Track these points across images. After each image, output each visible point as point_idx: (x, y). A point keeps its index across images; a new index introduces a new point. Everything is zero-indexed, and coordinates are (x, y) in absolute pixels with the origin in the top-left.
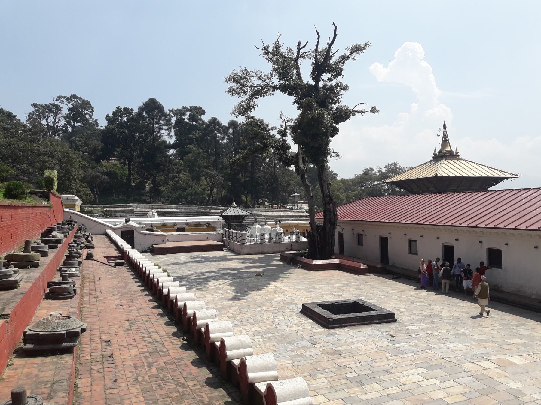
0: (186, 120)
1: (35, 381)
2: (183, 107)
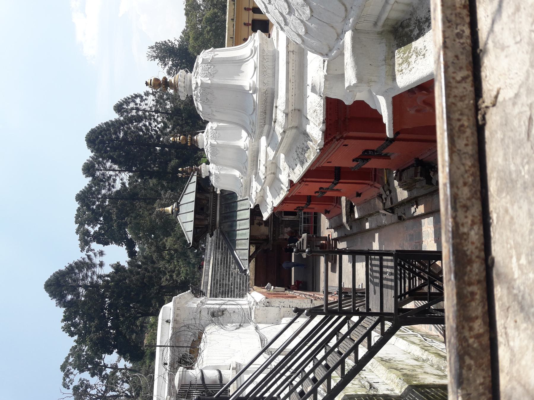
0: (97, 229)
1: (211, 30)
2: (77, 233)
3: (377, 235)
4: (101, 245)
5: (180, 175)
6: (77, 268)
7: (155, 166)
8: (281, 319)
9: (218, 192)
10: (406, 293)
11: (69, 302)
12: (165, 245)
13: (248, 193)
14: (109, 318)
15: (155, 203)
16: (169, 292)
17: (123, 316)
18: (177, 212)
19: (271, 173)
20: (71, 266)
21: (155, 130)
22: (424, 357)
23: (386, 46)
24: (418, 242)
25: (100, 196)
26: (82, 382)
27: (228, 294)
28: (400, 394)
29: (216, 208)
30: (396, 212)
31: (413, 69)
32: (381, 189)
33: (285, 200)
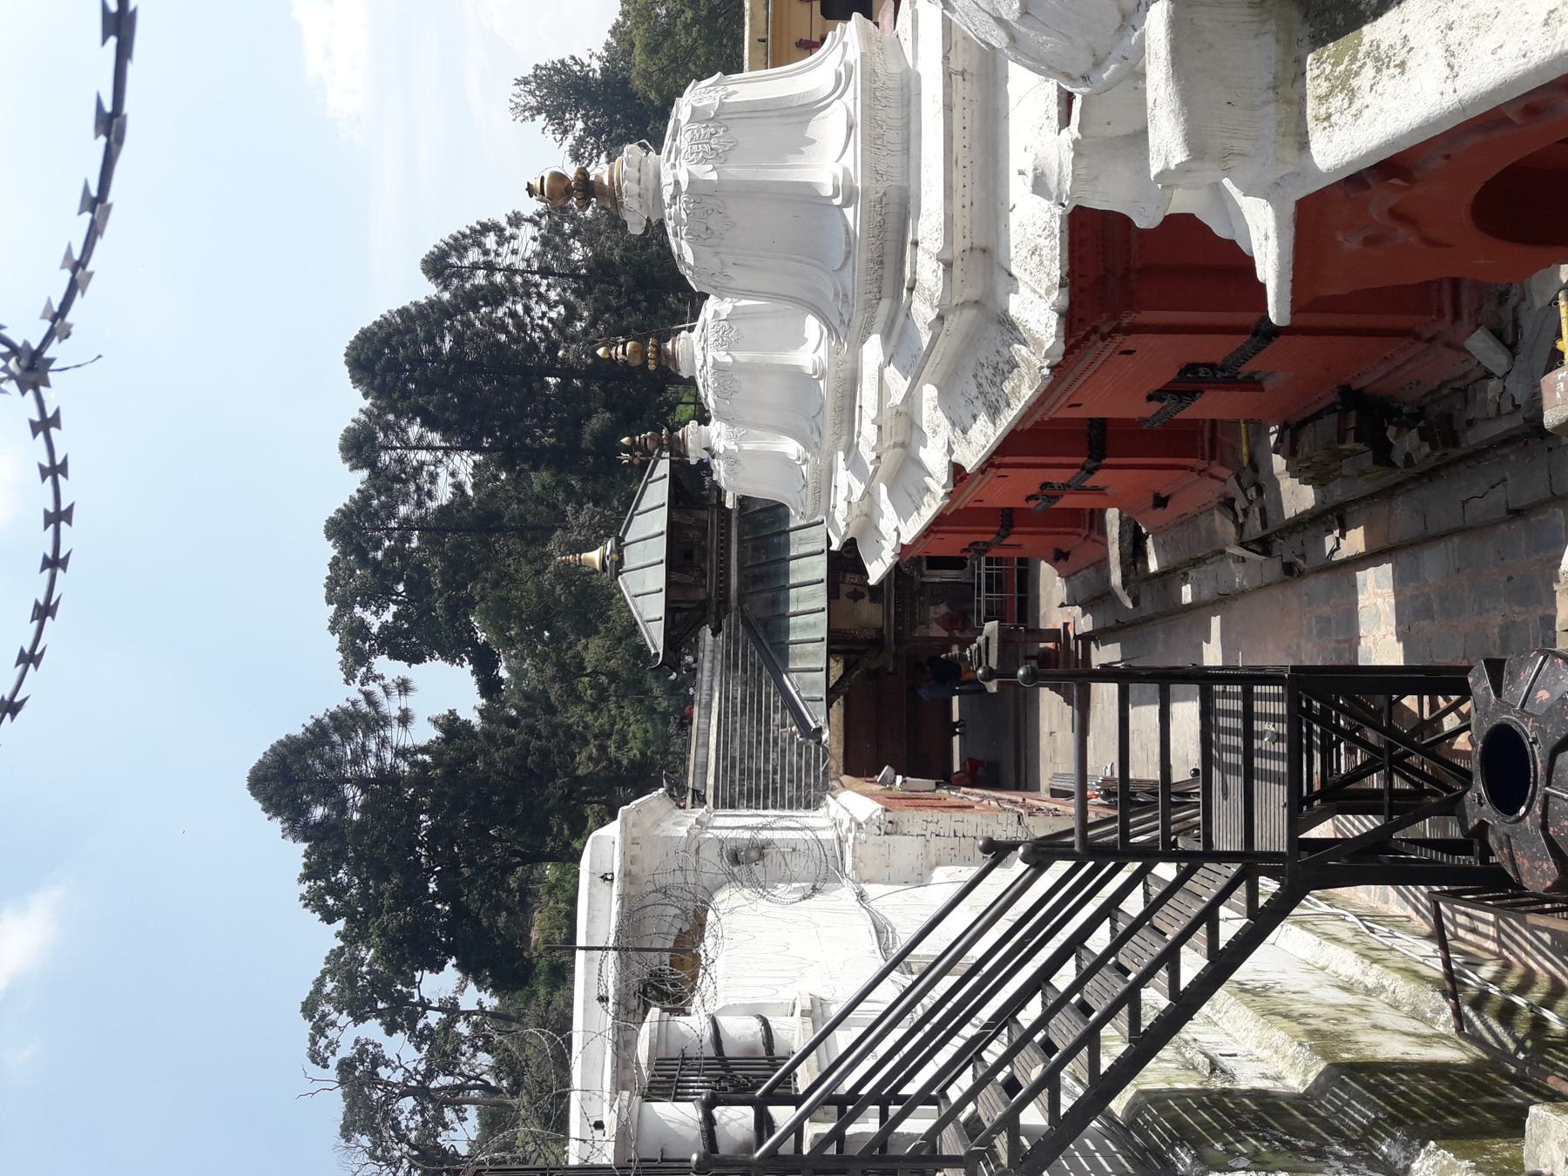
0: (388, 616)
1: (695, 21)
2: (333, 629)
3: (1216, 622)
4: (403, 664)
5: (625, 457)
6: (337, 729)
7: (545, 432)
8: (932, 869)
9: (729, 504)
10: (1313, 796)
11: (318, 825)
12: (583, 659)
13: (823, 506)
14: (430, 870)
15: (549, 540)
16: (599, 795)
17: (470, 862)
18: (617, 565)
19: (895, 445)
20: (318, 722)
21: (542, 327)
22: (1370, 981)
23: (1278, 41)
24: (1345, 641)
25: (393, 524)
26: (362, 1047)
27: (766, 798)
28: (1302, 1090)
29: (728, 550)
30: (1276, 552)
31: (1366, 113)
32: (1232, 482)
33: (938, 524)
